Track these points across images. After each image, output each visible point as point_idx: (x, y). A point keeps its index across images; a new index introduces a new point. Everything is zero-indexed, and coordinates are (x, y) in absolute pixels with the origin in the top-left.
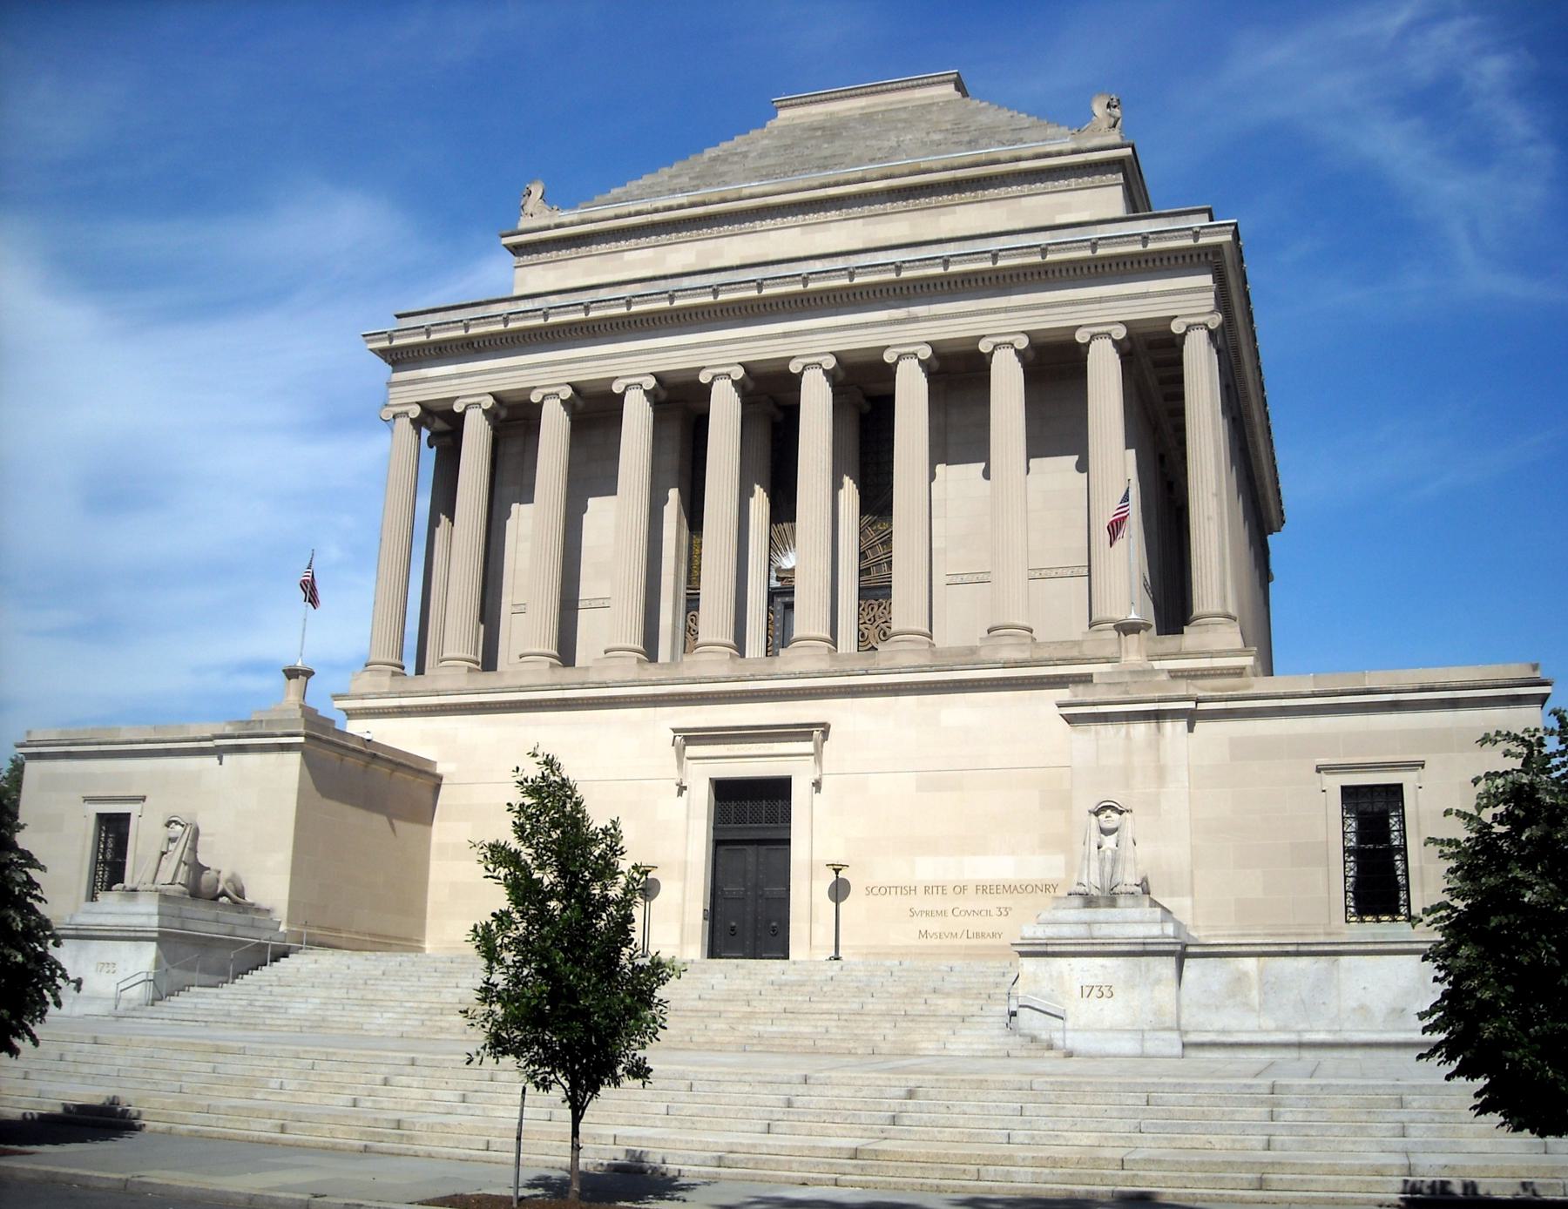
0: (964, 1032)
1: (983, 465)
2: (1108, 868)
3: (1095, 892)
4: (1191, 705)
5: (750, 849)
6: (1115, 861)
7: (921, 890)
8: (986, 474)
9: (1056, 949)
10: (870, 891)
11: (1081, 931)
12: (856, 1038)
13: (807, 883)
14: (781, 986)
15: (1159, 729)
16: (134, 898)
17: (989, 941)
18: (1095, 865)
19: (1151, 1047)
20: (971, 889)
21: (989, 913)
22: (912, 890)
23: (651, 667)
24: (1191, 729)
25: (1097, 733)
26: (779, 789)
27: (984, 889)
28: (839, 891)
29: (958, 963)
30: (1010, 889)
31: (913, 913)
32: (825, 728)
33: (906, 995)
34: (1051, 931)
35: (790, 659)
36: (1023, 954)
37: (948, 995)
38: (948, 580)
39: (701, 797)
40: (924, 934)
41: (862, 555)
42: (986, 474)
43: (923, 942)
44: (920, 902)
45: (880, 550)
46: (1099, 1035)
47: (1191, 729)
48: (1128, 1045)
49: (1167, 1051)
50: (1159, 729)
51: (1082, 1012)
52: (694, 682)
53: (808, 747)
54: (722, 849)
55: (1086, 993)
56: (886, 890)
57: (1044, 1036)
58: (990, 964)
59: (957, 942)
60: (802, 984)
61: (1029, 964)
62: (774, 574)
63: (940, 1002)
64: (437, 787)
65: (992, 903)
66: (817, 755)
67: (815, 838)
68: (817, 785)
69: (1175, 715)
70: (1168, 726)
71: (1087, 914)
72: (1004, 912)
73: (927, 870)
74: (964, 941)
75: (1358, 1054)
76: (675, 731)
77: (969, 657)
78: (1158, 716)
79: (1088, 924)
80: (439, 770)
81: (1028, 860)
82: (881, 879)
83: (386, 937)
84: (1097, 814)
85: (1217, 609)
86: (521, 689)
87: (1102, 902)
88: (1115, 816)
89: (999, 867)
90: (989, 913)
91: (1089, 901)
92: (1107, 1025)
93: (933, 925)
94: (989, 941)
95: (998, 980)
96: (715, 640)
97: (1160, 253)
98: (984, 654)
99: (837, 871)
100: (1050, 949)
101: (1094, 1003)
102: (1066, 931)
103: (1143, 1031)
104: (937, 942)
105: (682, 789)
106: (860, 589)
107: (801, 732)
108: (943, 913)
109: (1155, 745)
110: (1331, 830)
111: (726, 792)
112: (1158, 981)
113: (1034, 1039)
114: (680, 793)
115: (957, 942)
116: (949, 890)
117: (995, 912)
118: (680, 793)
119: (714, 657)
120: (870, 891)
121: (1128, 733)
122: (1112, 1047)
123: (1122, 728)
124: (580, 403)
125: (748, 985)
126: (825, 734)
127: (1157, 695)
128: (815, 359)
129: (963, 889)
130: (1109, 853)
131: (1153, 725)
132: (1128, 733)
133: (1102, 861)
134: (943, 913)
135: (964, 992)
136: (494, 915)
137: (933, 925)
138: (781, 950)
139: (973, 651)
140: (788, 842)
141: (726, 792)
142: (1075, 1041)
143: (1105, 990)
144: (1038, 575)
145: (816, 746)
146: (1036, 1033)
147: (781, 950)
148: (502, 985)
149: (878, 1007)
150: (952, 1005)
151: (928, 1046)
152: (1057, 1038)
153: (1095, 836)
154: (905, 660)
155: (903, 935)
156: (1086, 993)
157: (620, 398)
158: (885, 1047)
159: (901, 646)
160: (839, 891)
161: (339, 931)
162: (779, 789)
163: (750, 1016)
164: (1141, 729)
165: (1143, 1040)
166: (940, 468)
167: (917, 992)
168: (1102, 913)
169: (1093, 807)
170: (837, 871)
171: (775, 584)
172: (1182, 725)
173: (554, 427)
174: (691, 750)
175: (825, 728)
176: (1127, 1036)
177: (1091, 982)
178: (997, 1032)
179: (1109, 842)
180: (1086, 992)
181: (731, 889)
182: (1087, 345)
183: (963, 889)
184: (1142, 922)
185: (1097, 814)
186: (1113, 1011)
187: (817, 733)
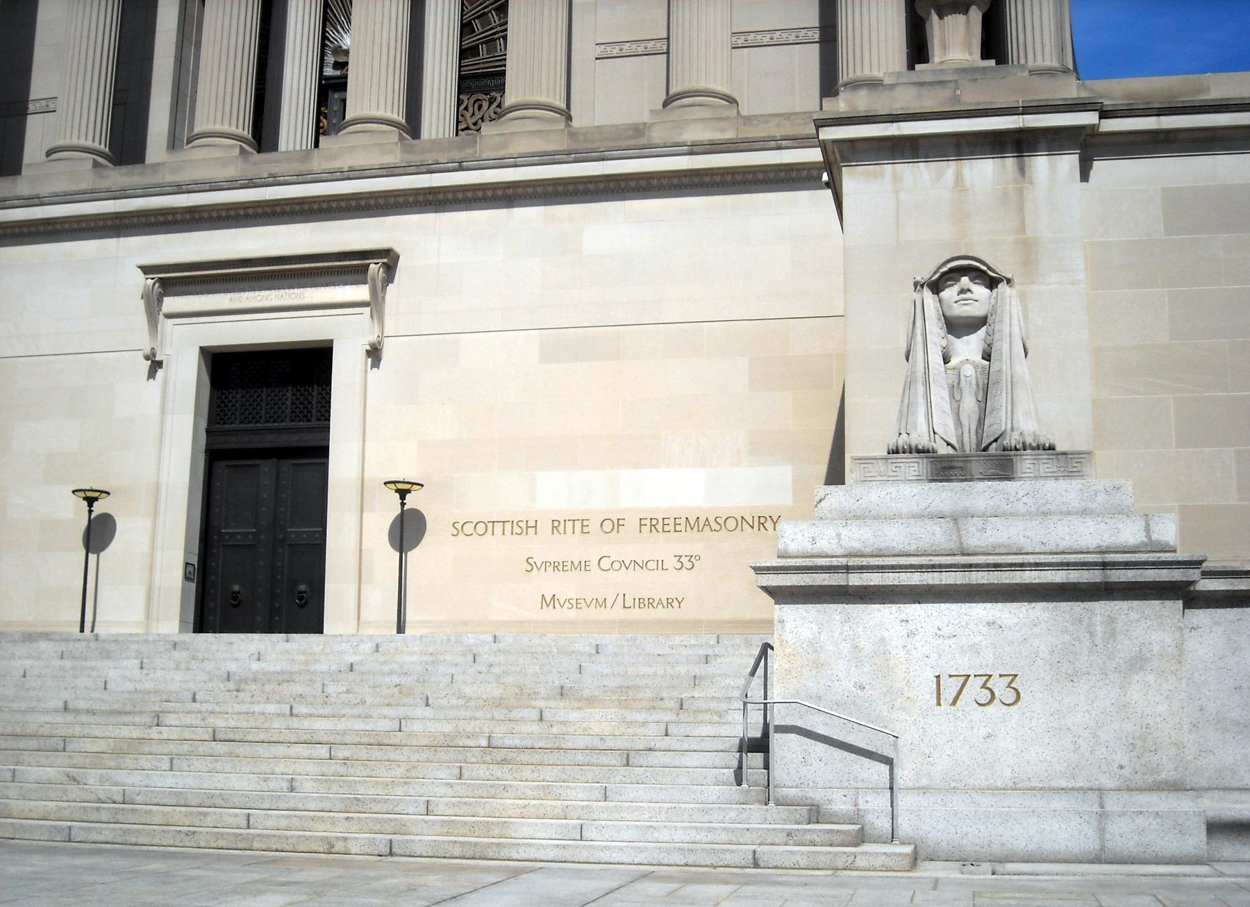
0: (632, 791)
2: (969, 404)
4: (1089, 118)
5: (266, 467)
6: (985, 391)
7: (545, 527)
9: (874, 579)
10: (459, 529)
11: (935, 535)
12: (354, 806)
13: (354, 517)
15: (1022, 170)
17: (661, 613)
18: (940, 395)
19: (1123, 834)
21: (661, 564)
22: (527, 527)
24: (1085, 176)
25: (896, 178)
26: (309, 367)
27: (654, 524)
28: (407, 530)
29: (610, 640)
30: (698, 524)
31: (531, 565)
32: (389, 259)
33: (499, 703)
34: (857, 537)
35: (342, 149)
36: (781, 595)
37: (591, 701)
38: (599, 51)
39: (186, 375)
40: (550, 602)
41: (466, 28)
43: (551, 614)
44: (544, 547)
45: (494, 19)
46: (985, 802)
47: (1085, 176)
48: (1065, 829)
49: (1171, 844)
50: (1022, 170)
51: (937, 742)
52: (179, 189)
53: (360, 292)
54: (221, 466)
55: (948, 695)
56: (489, 526)
57: (840, 805)
58: (677, 640)
61: (798, 624)
62: (330, 59)
63: (574, 716)
65: (665, 547)
66: (375, 304)
67: (368, 437)
68: (374, 353)
69: (1055, 140)
70: (1040, 164)
71: (947, 495)
72: (688, 562)
73: (556, 491)
74: (617, 613)
75: (821, 747)
76: (146, 270)
77: (634, 139)
78: (1019, 144)
79: (956, 518)
81: (726, 473)
82: (479, 505)
84: (936, 287)
87: (976, 467)
88: (980, 291)
89: (681, 488)
90: (661, 564)
91: (945, 468)
92: (1004, 775)
93: (566, 586)
94: (661, 613)
95: (696, 670)
96: (219, 128)
98: (657, 135)
99: (403, 494)
100: (855, 580)
101: (973, 720)
102: (896, 536)
103: (1100, 790)
105: (156, 365)
106: (462, 78)
108: (583, 566)
109: (1016, 200)
111: (228, 370)
112: (1138, 662)
113: (816, 813)
114: (152, 374)
116: (594, 526)
117: (671, 563)
118: (152, 374)
119: (215, 153)
120: (459, 529)
121: (959, 177)
122: (1020, 836)
123: (949, 169)
126: (390, 269)
129: (618, 524)
130: (968, 371)
131: (1010, 162)
132: (959, 177)
133: (955, 390)
134: (583, 566)
135: (625, 695)
137: (566, 586)
138: (314, 624)
139: (638, 130)
140: (322, 452)
141: (228, 370)
142: (924, 818)
143: (999, 685)
144: (744, 42)
145: (373, 292)
146: (817, 796)
147: (314, 624)
149: (433, 727)
150: (599, 722)
151: (537, 834)
152: (875, 806)
153: (935, 329)
154: (523, 146)
156: (948, 695)
158: (423, 837)
159: (517, 126)
160: (407, 530)
162: (309, 367)
164: (985, 172)
165: (1103, 816)
167: (524, 695)
168: (981, 494)
169: (926, 272)
170: (403, 494)
171: (329, 71)
172: (1069, 162)
174: (172, 303)
175: (389, 259)
176: (1058, 803)
177: (964, 664)
178: (714, 792)
179: (968, 348)
180: (949, 690)
181: (235, 530)
184: (1084, 512)
185: (936, 287)
186: (1019, 740)
187: (374, 268)
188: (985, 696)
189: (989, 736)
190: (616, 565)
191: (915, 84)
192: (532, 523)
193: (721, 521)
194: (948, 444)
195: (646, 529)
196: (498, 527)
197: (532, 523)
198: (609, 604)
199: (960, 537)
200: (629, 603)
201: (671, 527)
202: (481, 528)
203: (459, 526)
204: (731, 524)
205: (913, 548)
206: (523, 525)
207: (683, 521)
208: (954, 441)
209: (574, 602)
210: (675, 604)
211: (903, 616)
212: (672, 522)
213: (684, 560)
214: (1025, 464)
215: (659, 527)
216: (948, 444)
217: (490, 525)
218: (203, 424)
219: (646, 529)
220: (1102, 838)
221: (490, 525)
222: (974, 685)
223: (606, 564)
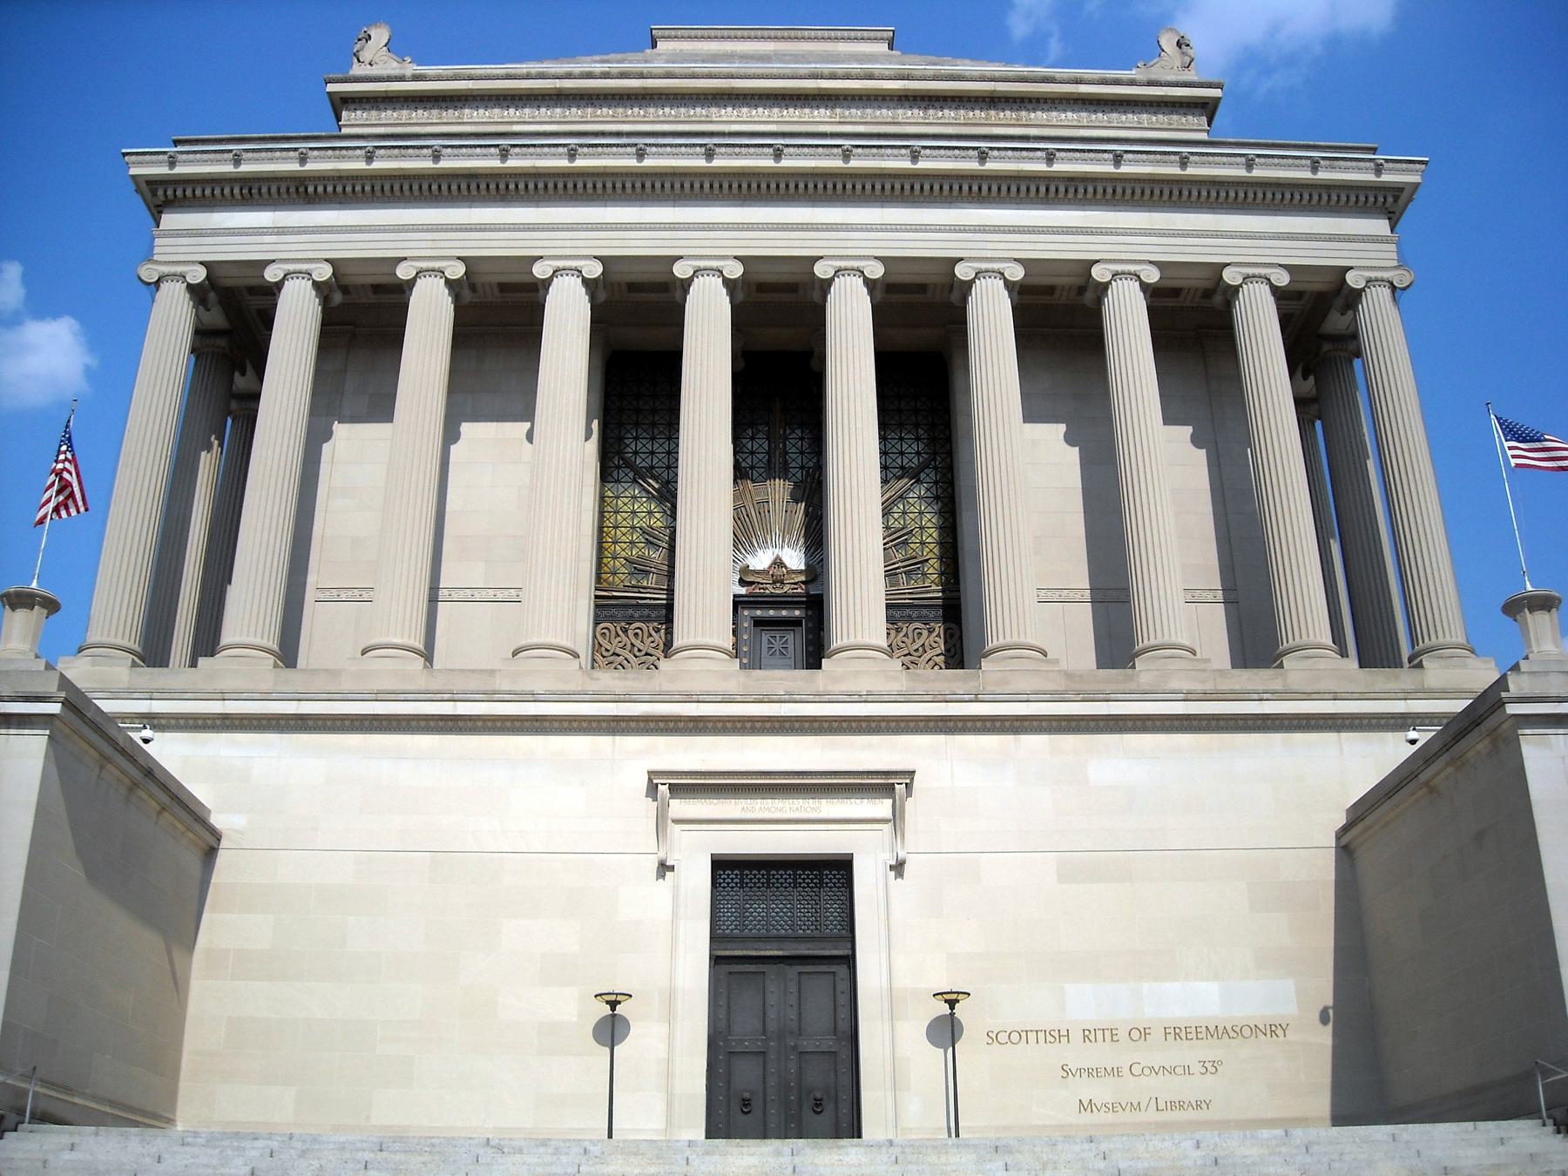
1: (528, 425)
7: (1076, 1036)
8: (530, 437)
10: (993, 1038)
16: (626, 1023)
20: (1157, 1034)
21: (1187, 1070)
22: (1058, 1036)
23: (288, 673)
27: (1177, 1033)
28: (946, 1031)
30: (1216, 1032)
39: (697, 880)
40: (1086, 1106)
42: (530, 437)
43: (1087, 1118)
44: (1077, 1054)
53: (883, 807)
59: (1139, 1117)
64: (211, 853)
65: (1190, 1054)
66: (897, 819)
67: (897, 953)
68: (898, 868)
73: (1084, 1003)
74: (1151, 1115)
80: (216, 820)
83: (132, 1110)
85: (1461, 640)
86: (688, 698)
93: (1100, 1091)
97: (1329, 187)
99: (613, 1005)
104: (1110, 1117)
105: (664, 868)
107: (883, 784)
108: (1116, 1072)
110: (670, 950)
115: (1139, 1117)
116: (1122, 1034)
120: (993, 1038)
124: (338, 298)
128: (304, 267)
129: (1145, 1033)
134: (1116, 1072)
137: (1100, 1091)
155: (1051, 1106)
157: (273, 290)
161: (67, 1090)
166: (466, 428)
173: (429, 323)
174: (681, 807)
182: (830, 282)
190: (1147, 1071)
196: (1032, 1036)
200: (1162, 1105)
215: (1183, 1035)
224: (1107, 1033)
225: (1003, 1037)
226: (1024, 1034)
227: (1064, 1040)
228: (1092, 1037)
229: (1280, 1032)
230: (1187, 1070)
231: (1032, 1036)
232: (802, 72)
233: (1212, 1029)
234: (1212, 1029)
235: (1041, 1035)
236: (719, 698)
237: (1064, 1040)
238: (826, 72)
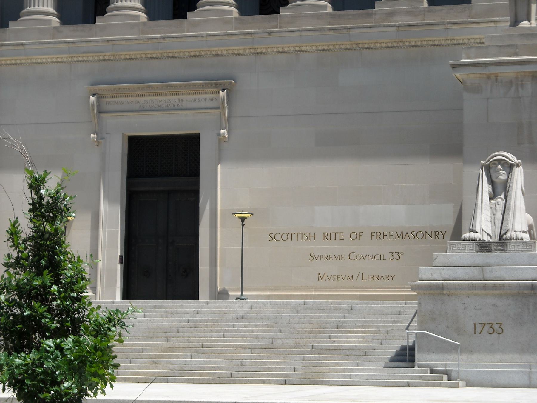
3: (487, 239)
7: (320, 236)
14: (195, 324)
21: (382, 257)
22: (311, 237)
27: (380, 235)
30: (401, 235)
44: (321, 247)
60: (216, 322)
65: (385, 247)
72: (397, 256)
102: (460, 271)
108: (340, 257)
117: (388, 256)
125: (166, 323)
127: (183, 40)
129: (358, 236)
134: (340, 257)
136: (79, 257)
143: (496, 327)
148: (43, 321)
150: (353, 340)
163: (170, 352)
168: (495, 255)
183: (358, 236)
188: (491, 331)
189: (492, 344)
190: (358, 257)
191: (497, 46)
192: (312, 234)
193: (414, 233)
194: (488, 234)
195: (374, 238)
196: (294, 236)
197: (312, 234)
198: (355, 278)
199: (483, 274)
200: (365, 277)
201: (388, 237)
202: (285, 237)
203: (272, 235)
204: (420, 235)
205: (467, 278)
206: (308, 235)
207: (394, 233)
208: (490, 233)
209: (336, 277)
210: (390, 278)
211: (463, 302)
212: (388, 234)
213: (395, 255)
214: (511, 245)
215: (382, 237)
216: (488, 234)
217: (290, 235)
218: (125, 176)
219: (374, 238)
220: (530, 381)
221: (290, 235)
222: (487, 328)
223: (353, 256)
224: (338, 235)
225: (278, 237)
226: (289, 236)
227: (312, 238)
228: (328, 237)
229: (440, 236)
230: (382, 257)
231: (294, 236)
232: (475, 24)
233: (399, 234)
234: (399, 234)
235: (300, 235)
236: (340, 384)
237: (312, 238)
238: (489, 23)
